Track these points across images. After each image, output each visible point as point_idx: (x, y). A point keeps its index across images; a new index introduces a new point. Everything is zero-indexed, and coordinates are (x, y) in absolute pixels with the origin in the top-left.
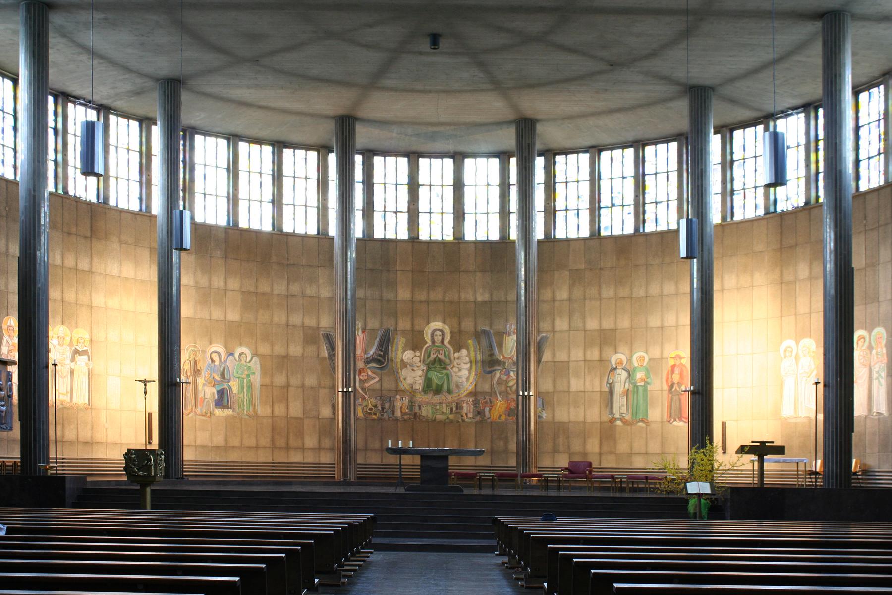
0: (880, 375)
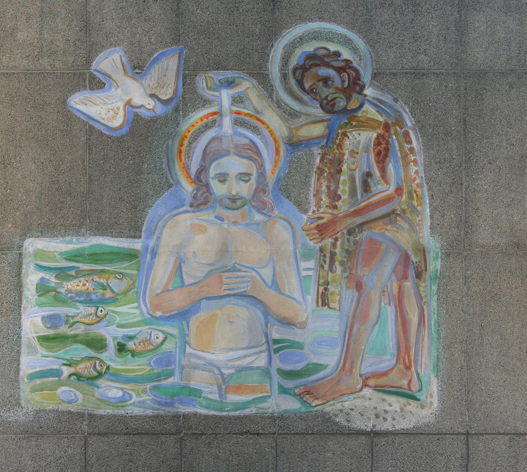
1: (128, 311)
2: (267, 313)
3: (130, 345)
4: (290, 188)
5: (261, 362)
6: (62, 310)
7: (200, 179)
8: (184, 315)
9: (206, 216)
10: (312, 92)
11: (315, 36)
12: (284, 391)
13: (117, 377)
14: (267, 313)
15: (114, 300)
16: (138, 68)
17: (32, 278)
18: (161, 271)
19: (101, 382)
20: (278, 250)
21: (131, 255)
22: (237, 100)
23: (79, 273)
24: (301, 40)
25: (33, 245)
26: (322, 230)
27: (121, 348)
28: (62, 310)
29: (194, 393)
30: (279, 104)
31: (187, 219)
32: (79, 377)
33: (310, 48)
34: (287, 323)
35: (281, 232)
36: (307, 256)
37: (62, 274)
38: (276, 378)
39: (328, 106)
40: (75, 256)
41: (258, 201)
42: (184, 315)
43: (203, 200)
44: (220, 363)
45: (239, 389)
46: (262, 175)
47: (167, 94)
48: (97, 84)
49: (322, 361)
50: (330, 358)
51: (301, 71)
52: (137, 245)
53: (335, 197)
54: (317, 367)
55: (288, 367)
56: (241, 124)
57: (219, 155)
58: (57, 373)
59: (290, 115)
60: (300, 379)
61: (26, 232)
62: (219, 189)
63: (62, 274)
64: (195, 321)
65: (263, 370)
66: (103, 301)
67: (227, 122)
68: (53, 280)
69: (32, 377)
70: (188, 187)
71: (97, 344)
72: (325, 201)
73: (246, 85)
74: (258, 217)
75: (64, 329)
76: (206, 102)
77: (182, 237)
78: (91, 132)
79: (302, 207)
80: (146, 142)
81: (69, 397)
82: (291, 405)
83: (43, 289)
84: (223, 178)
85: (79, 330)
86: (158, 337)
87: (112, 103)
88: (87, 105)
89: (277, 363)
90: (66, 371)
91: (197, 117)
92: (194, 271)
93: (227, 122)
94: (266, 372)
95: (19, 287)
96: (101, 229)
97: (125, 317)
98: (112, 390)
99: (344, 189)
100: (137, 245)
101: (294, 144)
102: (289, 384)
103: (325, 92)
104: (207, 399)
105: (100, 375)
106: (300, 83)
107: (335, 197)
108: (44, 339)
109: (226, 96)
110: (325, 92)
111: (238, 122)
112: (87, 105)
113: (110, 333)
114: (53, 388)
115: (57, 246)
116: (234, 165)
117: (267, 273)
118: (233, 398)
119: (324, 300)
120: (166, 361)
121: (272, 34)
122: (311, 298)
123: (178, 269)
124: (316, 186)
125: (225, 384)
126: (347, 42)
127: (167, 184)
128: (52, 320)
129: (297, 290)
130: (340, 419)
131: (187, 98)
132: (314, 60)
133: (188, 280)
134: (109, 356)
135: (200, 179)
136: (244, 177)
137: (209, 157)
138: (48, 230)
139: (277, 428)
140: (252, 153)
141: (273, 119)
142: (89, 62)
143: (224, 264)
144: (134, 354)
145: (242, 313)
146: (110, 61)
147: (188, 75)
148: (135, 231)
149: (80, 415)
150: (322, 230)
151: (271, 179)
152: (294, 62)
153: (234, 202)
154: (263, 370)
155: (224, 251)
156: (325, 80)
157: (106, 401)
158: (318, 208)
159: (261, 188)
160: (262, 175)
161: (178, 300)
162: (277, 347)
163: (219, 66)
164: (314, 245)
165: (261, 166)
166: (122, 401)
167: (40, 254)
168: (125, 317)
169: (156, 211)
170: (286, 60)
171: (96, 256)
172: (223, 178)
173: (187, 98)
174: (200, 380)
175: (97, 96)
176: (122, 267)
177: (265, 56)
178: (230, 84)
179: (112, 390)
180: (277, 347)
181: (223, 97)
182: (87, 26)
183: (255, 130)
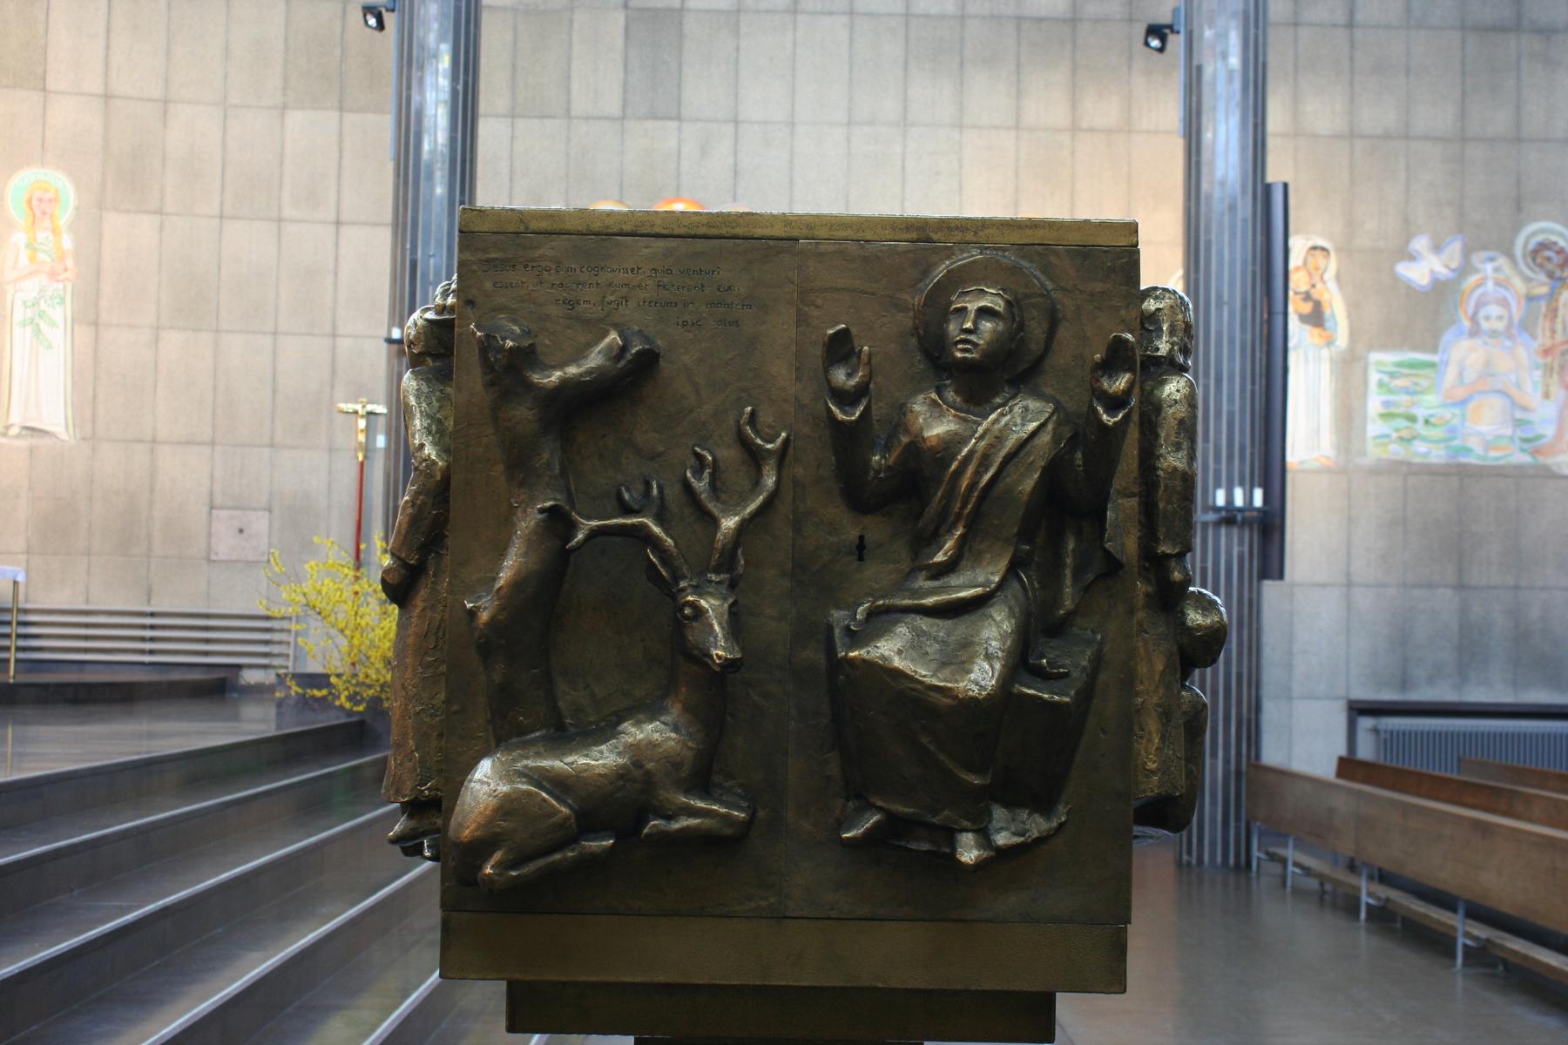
0: (41, 314)
1: (1431, 399)
2: (1513, 402)
3: (1432, 420)
4: (1527, 326)
5: (1509, 432)
6: (1392, 398)
7: (1474, 319)
8: (1463, 403)
9: (1477, 342)
10: (1541, 266)
11: (1543, 231)
12: (1522, 450)
13: (1425, 439)
14: (1513, 402)
15: (1422, 393)
16: (1437, 248)
17: (1374, 377)
18: (1450, 375)
19: (1416, 443)
20: (1520, 365)
21: (1432, 365)
22: (1497, 270)
23: (1402, 375)
24: (1534, 234)
25: (1375, 356)
26: (1546, 352)
27: (1427, 422)
28: (1392, 398)
29: (1468, 451)
30: (1521, 274)
31: (1466, 343)
32: (1401, 439)
33: (1540, 238)
34: (1524, 409)
35: (1522, 352)
36: (1537, 368)
37: (1392, 375)
38: (1518, 442)
39: (1551, 275)
40: (1400, 365)
41: (1508, 333)
42: (1463, 403)
43: (1475, 331)
44: (1485, 434)
45: (1495, 449)
46: (1510, 318)
47: (1454, 265)
48: (1412, 258)
49: (1541, 431)
50: (1549, 431)
51: (1535, 252)
52: (1435, 358)
53: (1553, 331)
54: (1540, 437)
55: (1525, 436)
56: (1499, 284)
57: (1485, 304)
58: (1388, 436)
59: (1527, 280)
60: (1531, 443)
61: (1371, 348)
62: (1485, 325)
63: (1392, 375)
64: (1471, 406)
65: (1019, 94)
66: (1415, 393)
67: (1490, 285)
68: (1386, 379)
69: (1375, 438)
70: (1466, 324)
71: (1412, 419)
72: (1548, 333)
73: (1502, 261)
74: (1508, 343)
75: (1393, 410)
76: (1477, 271)
77: (1464, 354)
78: (1410, 289)
79: (1534, 337)
80: (1442, 293)
81: (1395, 451)
82: (1525, 459)
83: (1381, 384)
84: (1487, 318)
85: (1401, 410)
86: (1448, 416)
87: (1422, 270)
88: (1406, 270)
89: (1519, 433)
90: (1394, 435)
91: (1472, 280)
92: (1470, 376)
93: (1490, 285)
94: (1512, 439)
95: (1365, 382)
96: (1415, 348)
97: (1429, 403)
98: (1421, 447)
99: (1559, 327)
100: (1435, 358)
101: (1530, 299)
102: (1526, 446)
103: (1550, 266)
104: (1477, 456)
105: (1414, 438)
106: (1534, 260)
107: (1553, 331)
108: (1382, 416)
109: (1489, 267)
110: (1550, 266)
111: (1498, 283)
112: (1406, 270)
113: (1420, 413)
114: (1386, 445)
115: (1389, 358)
116: (1494, 310)
117: (1513, 377)
118: (1493, 454)
119: (1546, 395)
120: (1453, 431)
121: (1517, 228)
122: (1539, 394)
123: (1460, 375)
124: (1542, 325)
125: (1488, 446)
126: (1561, 235)
127: (1454, 321)
128: (1386, 404)
129: (1530, 385)
130: (1555, 468)
131: (1465, 269)
132: (1543, 246)
133: (1467, 381)
134: (1419, 427)
135: (1474, 319)
136: (1500, 318)
137: (1480, 305)
138: (1384, 347)
139: (1516, 474)
140: (1504, 303)
141: (1518, 283)
142: (1407, 242)
143: (1488, 371)
144: (1434, 425)
145: (1498, 402)
146: (1420, 244)
147: (1467, 253)
148: (1434, 349)
149: (1402, 463)
150: (1546, 352)
151: (1516, 319)
152: (1531, 246)
153: (1494, 333)
154: (1019, 94)
155: (1488, 363)
156: (1549, 259)
157: (1417, 454)
158: (1542, 339)
159: (1510, 326)
160: (1510, 318)
161: (1461, 393)
162: (1518, 423)
163: (1485, 248)
164: (1541, 361)
165: (1510, 311)
166: (1426, 455)
167: (1379, 363)
168: (1429, 403)
169: (1447, 337)
170: (1525, 246)
171: (1412, 365)
172: (1487, 318)
173: (1465, 269)
174: (1473, 443)
175: (1412, 265)
176: (1428, 372)
177: (1512, 243)
178: (1492, 259)
179: (1421, 447)
180: (1518, 423)
181: (1489, 269)
182: (1406, 221)
183: (1506, 288)
